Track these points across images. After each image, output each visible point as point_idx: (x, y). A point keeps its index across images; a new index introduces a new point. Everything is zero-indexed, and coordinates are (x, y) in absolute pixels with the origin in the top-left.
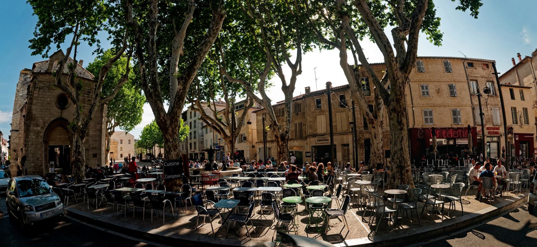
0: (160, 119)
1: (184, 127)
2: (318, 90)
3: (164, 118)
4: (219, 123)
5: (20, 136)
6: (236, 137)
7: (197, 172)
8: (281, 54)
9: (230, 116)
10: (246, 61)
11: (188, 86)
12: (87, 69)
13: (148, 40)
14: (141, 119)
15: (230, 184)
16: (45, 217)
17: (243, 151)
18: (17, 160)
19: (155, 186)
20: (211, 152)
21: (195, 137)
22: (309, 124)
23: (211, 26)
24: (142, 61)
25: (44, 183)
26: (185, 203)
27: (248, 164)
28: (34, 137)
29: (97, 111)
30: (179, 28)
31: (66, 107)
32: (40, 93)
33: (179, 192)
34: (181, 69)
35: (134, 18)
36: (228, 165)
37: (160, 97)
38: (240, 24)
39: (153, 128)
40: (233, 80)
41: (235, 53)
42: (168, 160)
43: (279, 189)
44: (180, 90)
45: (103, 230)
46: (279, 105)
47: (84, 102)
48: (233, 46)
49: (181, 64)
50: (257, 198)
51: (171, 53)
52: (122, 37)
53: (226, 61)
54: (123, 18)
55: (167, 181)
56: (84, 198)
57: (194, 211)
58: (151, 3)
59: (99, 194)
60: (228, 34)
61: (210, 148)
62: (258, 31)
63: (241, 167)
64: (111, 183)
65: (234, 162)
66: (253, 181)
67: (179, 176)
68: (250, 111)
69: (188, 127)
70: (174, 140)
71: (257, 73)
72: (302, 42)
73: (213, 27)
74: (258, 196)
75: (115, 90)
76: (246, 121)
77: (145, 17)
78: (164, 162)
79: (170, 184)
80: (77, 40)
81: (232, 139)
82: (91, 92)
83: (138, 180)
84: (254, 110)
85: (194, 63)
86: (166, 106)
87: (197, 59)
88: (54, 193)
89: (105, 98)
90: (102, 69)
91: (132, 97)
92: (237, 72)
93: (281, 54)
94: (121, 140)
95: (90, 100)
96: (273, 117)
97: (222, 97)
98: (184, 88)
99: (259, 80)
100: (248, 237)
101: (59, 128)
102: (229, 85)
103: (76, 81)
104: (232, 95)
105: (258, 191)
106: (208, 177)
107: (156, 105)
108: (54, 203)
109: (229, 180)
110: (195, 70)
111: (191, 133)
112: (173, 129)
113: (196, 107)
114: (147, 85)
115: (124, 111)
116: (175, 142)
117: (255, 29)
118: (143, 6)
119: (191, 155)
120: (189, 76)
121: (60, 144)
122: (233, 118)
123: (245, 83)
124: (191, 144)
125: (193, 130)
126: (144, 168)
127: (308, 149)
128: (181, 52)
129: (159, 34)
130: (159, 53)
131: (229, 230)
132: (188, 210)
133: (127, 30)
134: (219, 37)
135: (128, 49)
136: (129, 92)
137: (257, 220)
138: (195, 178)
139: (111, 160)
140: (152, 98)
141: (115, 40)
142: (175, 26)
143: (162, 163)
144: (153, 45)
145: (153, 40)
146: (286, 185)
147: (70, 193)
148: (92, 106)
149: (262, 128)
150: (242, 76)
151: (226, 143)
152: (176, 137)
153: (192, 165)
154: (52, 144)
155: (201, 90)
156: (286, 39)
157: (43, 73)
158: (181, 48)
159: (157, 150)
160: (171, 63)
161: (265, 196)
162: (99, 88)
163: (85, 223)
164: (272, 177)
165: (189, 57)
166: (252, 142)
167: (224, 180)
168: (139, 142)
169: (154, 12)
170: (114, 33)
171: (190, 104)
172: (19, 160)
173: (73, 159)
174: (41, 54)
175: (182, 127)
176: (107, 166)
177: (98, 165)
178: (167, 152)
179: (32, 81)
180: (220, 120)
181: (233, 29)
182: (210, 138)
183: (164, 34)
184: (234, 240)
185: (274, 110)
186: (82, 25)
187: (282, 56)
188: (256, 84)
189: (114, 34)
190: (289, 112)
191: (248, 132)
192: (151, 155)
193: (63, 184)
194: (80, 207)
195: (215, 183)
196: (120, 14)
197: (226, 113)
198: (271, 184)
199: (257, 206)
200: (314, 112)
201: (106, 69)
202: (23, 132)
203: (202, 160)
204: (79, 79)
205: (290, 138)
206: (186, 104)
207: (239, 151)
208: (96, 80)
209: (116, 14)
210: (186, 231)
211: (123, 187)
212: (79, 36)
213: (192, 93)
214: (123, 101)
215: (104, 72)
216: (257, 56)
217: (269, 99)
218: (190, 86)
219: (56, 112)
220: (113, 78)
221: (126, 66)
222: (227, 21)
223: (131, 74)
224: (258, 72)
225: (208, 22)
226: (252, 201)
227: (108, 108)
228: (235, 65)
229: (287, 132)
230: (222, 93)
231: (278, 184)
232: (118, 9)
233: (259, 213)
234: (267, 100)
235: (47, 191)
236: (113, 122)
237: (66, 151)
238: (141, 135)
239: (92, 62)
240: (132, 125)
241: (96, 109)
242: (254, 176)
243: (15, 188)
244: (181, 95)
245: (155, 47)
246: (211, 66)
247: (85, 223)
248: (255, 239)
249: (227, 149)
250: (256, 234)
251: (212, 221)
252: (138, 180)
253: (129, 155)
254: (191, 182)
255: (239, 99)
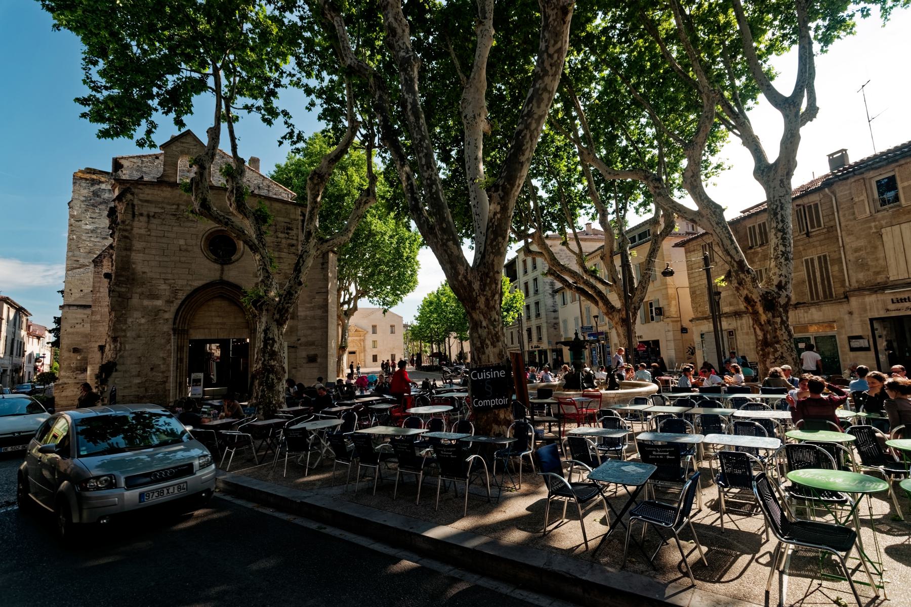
0: (457, 280)
1: (511, 293)
2: (884, 149)
3: (465, 277)
4: (592, 280)
5: (98, 317)
6: (636, 309)
7: (545, 392)
8: (744, 78)
9: (617, 261)
10: (643, 121)
11: (512, 204)
12: (272, 177)
13: (404, 107)
14: (415, 282)
15: (628, 423)
16: (154, 499)
17: (656, 343)
18: (85, 370)
19: (450, 424)
20: (577, 346)
21: (538, 315)
22: (851, 257)
23: (542, 45)
24: (399, 155)
25: (168, 420)
26: (517, 466)
27: (672, 374)
28: (143, 321)
29: (313, 267)
30: (468, 68)
31: (234, 258)
32: (153, 226)
33: (505, 438)
34: (490, 165)
35: (357, 52)
36: (621, 377)
37: (452, 234)
38: (615, 20)
39: (444, 299)
40: (617, 174)
41: (613, 105)
42: (478, 366)
43: (773, 443)
44: (495, 214)
45: (314, 526)
46: (749, 216)
47: (278, 247)
48: (605, 89)
49: (488, 155)
50: (705, 464)
51: (462, 132)
52: (342, 103)
53: (593, 130)
54: (331, 56)
55: (477, 411)
56: (278, 450)
57: (538, 485)
58: (385, 8)
59: (317, 442)
60: (588, 57)
61: (574, 337)
62: (666, 25)
63: (654, 381)
64: (349, 417)
65: (636, 369)
66: (690, 417)
67: (504, 401)
68: (667, 244)
69: (520, 294)
70: (492, 322)
71: (678, 145)
72: (814, 15)
73: (547, 47)
74: (707, 458)
75: (349, 223)
76: (658, 270)
77: (381, 47)
78: (471, 370)
79: (484, 420)
80: (228, 110)
81: (627, 314)
82: (294, 226)
83: (413, 410)
84: (678, 240)
85: (518, 149)
86: (469, 252)
87: (524, 137)
88: (195, 442)
89: (327, 241)
90: (312, 176)
91: (391, 237)
92: (624, 152)
93: (744, 78)
94: (374, 327)
95: (293, 245)
96: (733, 252)
97: (593, 218)
98: (504, 209)
99: (684, 163)
100: (686, 575)
101: (217, 303)
102: (607, 190)
103: (250, 203)
104: (617, 211)
105: (706, 445)
106: (573, 403)
107: (446, 251)
108: (191, 466)
109: (624, 414)
110: (522, 164)
111: (528, 307)
112: (487, 300)
113: (534, 248)
114: (421, 210)
115: (376, 265)
116: (495, 327)
117: (659, 22)
118: (370, 14)
119: (531, 354)
120: (511, 179)
121: (222, 336)
122: (625, 265)
123: (646, 178)
124: (529, 331)
125: (532, 300)
126: (426, 385)
127: (857, 327)
128: (483, 126)
129: (425, 88)
130: (435, 136)
131: (630, 546)
132: (525, 481)
133: (348, 85)
134: (567, 71)
135: (364, 132)
136: (383, 226)
137: (711, 527)
138: (541, 406)
139: (351, 367)
140: (436, 236)
141: (325, 110)
142: (457, 63)
143: (466, 372)
144: (417, 118)
145: (414, 104)
146: (796, 435)
147: (243, 441)
148: (301, 256)
149: (706, 281)
150: (637, 161)
151: (613, 324)
152: (494, 316)
153: (533, 377)
154: (197, 335)
155: (542, 208)
156: (754, 28)
157: (150, 184)
158: (483, 117)
159: (454, 346)
160: (466, 156)
161: (729, 461)
162: (311, 219)
163: (269, 511)
164: (746, 408)
165: (505, 136)
166: (679, 319)
167: (612, 414)
168: (413, 329)
169: (399, 31)
170: (320, 93)
171: (522, 243)
172: (90, 374)
173: (256, 367)
174: (131, 137)
175: (507, 294)
176: (340, 381)
177: (320, 380)
178: (478, 350)
179: (119, 198)
180: (593, 273)
181: (598, 38)
182: (573, 314)
183: (436, 87)
184: (645, 579)
185: (736, 232)
186: (230, 73)
187: (746, 86)
188: (676, 175)
189: (319, 96)
190: (783, 231)
191: (667, 297)
192: (442, 357)
193: (224, 421)
194: (264, 472)
195: (590, 419)
196: (319, 45)
197: (607, 255)
198: (744, 427)
199: (706, 485)
200: (872, 218)
201: (320, 177)
202: (107, 310)
203: (557, 366)
204: (258, 199)
205: (794, 300)
206: (512, 244)
207: (647, 343)
208: (301, 201)
209: (308, 41)
210: (517, 536)
211: (375, 425)
212: (229, 100)
213: (523, 217)
214: (372, 246)
215: (318, 184)
216: (674, 100)
217: (719, 207)
218: (517, 202)
219: (206, 270)
220: (341, 197)
221: (365, 169)
222: (580, 22)
223: (381, 187)
224: (678, 140)
225: (534, 34)
226: (691, 470)
227: (339, 260)
228: (617, 137)
229: (780, 286)
230: (593, 210)
231: (766, 428)
232: (311, 29)
233: (715, 506)
234: (713, 210)
235: (176, 438)
236: (352, 289)
237: (236, 353)
238: (418, 314)
239: (283, 162)
240: (397, 295)
241: (310, 262)
242: (693, 406)
243: (66, 437)
244: (499, 225)
245: (422, 121)
246: (558, 148)
247: (269, 511)
248: (708, 585)
249: (616, 338)
250: (711, 570)
251: (585, 515)
252: (413, 410)
253: (393, 357)
254: (532, 414)
255: (634, 218)
